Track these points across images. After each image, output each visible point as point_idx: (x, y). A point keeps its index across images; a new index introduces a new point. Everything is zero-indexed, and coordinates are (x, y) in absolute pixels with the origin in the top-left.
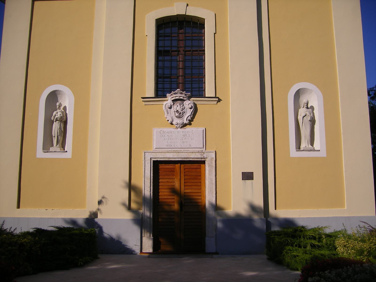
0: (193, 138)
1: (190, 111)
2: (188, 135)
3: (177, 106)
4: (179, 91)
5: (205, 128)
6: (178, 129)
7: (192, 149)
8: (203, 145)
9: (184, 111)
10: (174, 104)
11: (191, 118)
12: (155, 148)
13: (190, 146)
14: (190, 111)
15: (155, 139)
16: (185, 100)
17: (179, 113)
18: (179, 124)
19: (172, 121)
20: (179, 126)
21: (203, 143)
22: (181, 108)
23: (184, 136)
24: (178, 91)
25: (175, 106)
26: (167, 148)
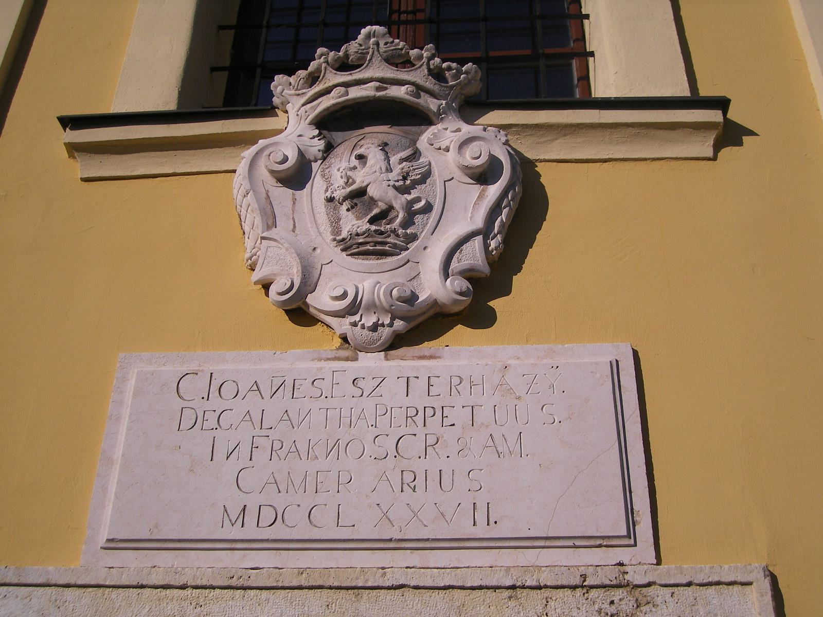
0: (512, 438)
1: (481, 197)
2: (459, 415)
3: (354, 162)
4: (377, 44)
5: (635, 353)
6: (356, 359)
7: (507, 558)
8: (630, 511)
9: (418, 200)
10: (329, 148)
11: (491, 263)
12: (102, 541)
13: (481, 517)
14: (481, 197)
15: (118, 453)
16: (423, 119)
17: (376, 211)
18: (373, 307)
19: (308, 284)
20: (375, 328)
21: (627, 490)
22: (389, 170)
23: (419, 419)
24: (368, 36)
25: (341, 162)
26: (231, 544)
